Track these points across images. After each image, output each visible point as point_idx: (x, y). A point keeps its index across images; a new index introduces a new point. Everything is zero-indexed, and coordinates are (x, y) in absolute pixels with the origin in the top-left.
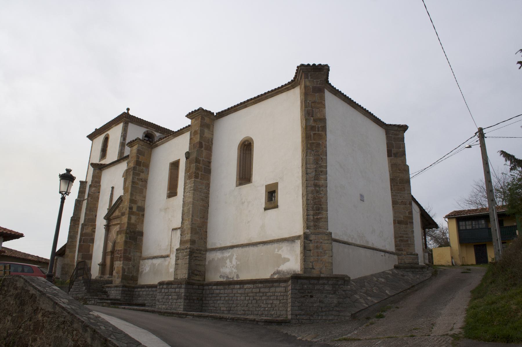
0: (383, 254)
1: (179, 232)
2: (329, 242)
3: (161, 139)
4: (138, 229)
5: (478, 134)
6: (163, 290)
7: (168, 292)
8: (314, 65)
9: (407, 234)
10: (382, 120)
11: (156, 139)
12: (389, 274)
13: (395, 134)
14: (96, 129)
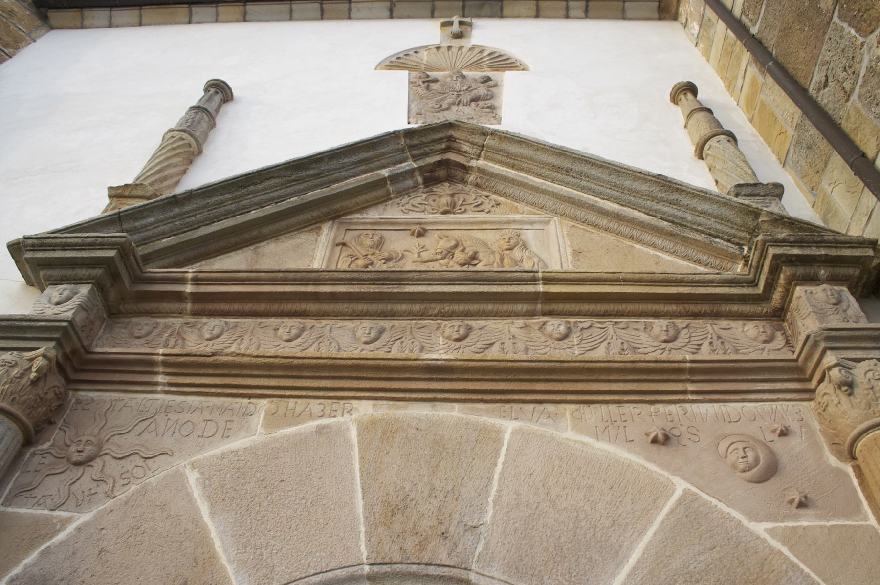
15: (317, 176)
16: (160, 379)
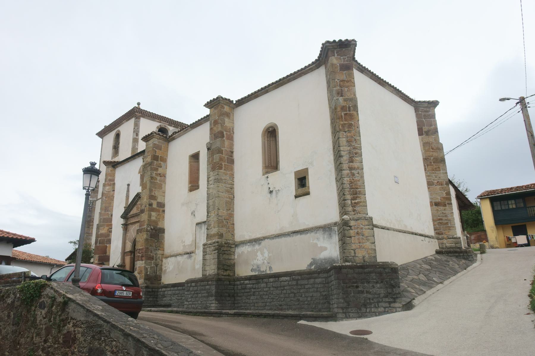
0: (423, 238)
1: (204, 227)
2: (371, 227)
3: (175, 133)
4: (160, 226)
6: (191, 289)
7: (197, 290)
8: (340, 41)
9: (446, 216)
10: (411, 97)
11: (170, 133)
12: (432, 259)
13: (424, 111)
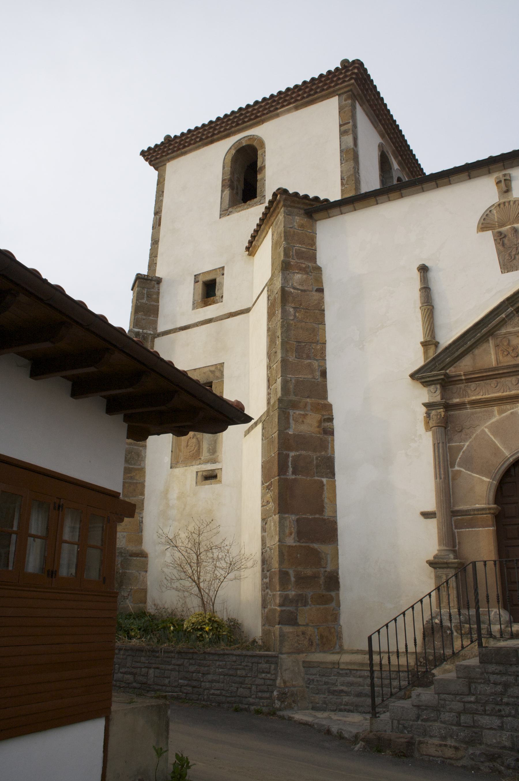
5: (266, 289)
14: (168, 137)
15: (483, 325)
16: (468, 406)
